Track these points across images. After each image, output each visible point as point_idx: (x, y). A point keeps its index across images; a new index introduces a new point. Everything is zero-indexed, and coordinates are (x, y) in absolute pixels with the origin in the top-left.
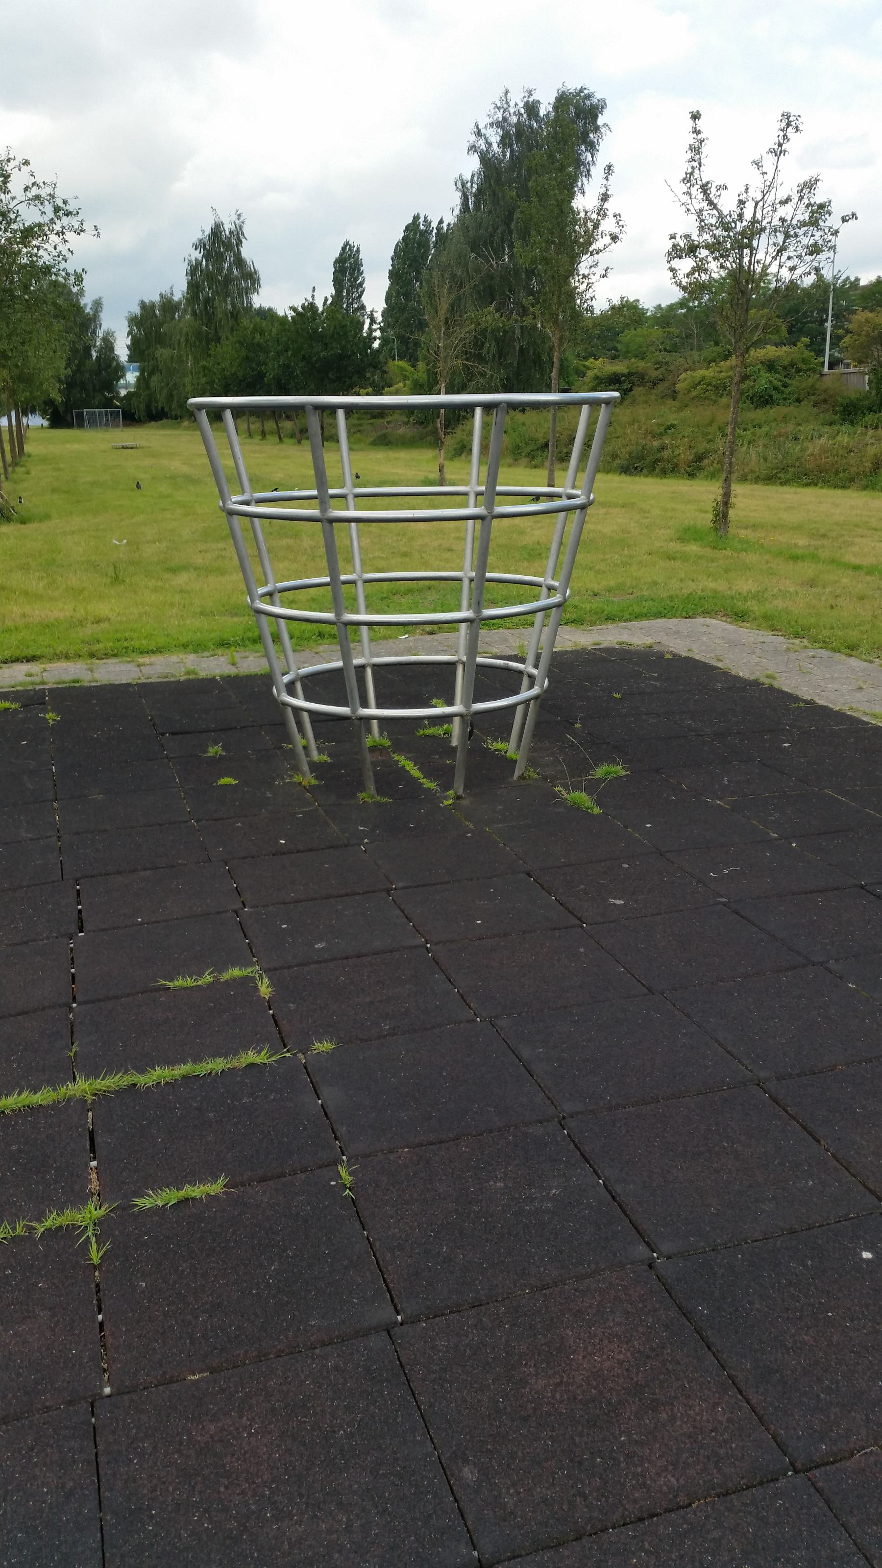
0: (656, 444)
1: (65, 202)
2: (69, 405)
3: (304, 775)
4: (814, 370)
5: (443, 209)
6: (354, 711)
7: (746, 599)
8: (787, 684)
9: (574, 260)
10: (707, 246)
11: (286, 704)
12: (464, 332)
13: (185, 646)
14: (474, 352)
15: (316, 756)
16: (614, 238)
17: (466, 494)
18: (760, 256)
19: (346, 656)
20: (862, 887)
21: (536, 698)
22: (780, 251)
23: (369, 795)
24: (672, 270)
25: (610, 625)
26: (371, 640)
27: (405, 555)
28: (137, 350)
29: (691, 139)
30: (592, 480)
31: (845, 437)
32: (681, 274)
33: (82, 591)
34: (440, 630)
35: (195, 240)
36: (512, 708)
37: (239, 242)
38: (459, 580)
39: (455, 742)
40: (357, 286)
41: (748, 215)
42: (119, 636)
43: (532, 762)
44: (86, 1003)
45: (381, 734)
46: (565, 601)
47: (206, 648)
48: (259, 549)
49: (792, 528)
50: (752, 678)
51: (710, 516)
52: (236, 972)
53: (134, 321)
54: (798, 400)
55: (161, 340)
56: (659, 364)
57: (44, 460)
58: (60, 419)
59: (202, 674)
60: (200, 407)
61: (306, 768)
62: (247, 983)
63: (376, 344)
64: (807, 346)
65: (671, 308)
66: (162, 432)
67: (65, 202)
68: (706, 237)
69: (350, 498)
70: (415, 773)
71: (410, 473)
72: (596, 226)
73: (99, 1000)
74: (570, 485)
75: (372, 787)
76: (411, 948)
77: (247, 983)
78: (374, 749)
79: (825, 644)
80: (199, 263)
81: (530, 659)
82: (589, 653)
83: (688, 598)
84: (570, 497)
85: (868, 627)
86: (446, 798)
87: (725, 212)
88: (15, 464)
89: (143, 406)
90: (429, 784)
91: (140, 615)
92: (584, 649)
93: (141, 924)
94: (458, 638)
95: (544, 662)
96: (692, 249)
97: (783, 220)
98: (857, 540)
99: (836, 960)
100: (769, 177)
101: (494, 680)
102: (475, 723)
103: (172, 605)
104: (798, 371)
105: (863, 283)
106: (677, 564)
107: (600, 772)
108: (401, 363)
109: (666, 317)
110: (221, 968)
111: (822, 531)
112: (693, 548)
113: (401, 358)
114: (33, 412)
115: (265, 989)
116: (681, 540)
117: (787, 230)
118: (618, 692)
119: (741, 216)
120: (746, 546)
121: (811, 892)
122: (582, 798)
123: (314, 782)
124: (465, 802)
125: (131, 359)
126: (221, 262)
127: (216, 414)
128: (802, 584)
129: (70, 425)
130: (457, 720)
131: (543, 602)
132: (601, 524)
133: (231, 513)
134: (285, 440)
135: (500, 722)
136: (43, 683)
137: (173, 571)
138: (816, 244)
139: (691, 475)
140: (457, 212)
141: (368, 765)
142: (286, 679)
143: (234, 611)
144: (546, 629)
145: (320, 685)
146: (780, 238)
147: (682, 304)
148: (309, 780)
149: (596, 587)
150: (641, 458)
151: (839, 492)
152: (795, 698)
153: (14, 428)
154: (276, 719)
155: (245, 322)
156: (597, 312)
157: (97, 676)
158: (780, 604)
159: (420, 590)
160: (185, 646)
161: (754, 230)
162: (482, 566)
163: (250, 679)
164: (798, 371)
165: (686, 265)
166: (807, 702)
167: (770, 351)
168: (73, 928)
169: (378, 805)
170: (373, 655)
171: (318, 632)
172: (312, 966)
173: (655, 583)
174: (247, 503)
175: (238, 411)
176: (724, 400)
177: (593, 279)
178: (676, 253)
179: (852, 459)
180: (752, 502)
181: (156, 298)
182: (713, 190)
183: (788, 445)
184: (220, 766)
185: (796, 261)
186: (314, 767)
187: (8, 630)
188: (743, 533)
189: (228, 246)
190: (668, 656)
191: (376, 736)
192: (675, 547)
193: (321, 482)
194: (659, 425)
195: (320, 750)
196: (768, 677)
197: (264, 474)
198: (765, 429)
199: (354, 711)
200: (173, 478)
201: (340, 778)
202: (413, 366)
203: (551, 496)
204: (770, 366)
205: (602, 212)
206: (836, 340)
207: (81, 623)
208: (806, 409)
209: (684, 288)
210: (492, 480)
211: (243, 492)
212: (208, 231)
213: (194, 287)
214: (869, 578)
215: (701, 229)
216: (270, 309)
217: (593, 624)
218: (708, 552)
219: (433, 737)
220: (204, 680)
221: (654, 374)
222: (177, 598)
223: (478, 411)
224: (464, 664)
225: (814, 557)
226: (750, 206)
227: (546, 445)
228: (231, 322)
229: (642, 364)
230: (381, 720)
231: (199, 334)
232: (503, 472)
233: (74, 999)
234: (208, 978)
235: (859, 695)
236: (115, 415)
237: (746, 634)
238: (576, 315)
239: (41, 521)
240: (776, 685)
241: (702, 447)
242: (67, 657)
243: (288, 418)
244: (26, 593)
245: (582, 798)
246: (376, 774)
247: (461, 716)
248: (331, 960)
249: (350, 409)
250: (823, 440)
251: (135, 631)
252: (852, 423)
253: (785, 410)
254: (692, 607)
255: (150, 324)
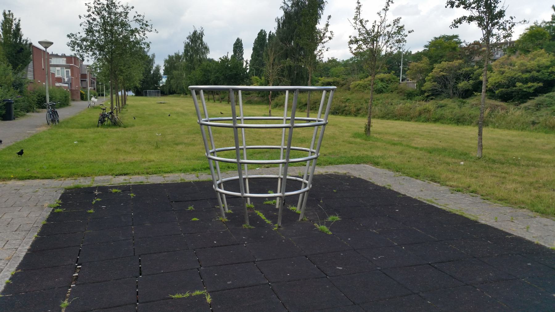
0: (343, 105)
1: (147, 22)
2: (142, 89)
3: (223, 217)
4: (397, 82)
5: (271, 28)
6: (242, 194)
7: (378, 158)
8: (395, 188)
9: (316, 45)
10: (361, 40)
11: (217, 192)
12: (278, 68)
13: (181, 170)
14: (281, 74)
15: (227, 211)
16: (330, 38)
17: (282, 119)
18: (380, 43)
19: (240, 175)
20: (430, 264)
21: (307, 191)
22: (387, 42)
23: (246, 225)
24: (350, 47)
25: (330, 166)
26: (248, 169)
27: (258, 140)
28: (167, 71)
29: (357, 5)
30: (327, 116)
31: (409, 104)
32: (353, 50)
33: (145, 151)
34: (271, 166)
35: (187, 36)
36: (298, 194)
37: (202, 36)
38: (280, 149)
39: (277, 207)
40: (241, 52)
41: (376, 30)
42: (157, 166)
43: (305, 214)
44: (142, 303)
45: (251, 203)
46: (318, 157)
47: (188, 171)
48: (210, 137)
49: (392, 134)
50: (383, 186)
51: (364, 129)
52: (198, 292)
53: (166, 61)
54: (392, 92)
55: (175, 68)
56: (344, 79)
57: (132, 107)
58: (139, 93)
59: (187, 180)
60: (193, 89)
61: (224, 215)
62: (202, 297)
63: (248, 71)
64: (394, 74)
65: (347, 61)
66: (176, 98)
67: (147, 22)
68: (361, 37)
69: (242, 120)
70: (263, 217)
71: (259, 113)
72: (324, 34)
73: (147, 302)
74: (318, 117)
75: (248, 222)
76: (263, 284)
77: (202, 297)
78: (249, 208)
79: (408, 175)
80: (189, 44)
81: (305, 177)
82: (324, 175)
83: (358, 157)
84: (319, 121)
85: (422, 169)
86: (275, 227)
87: (368, 29)
88: (123, 108)
89: (167, 90)
90: (268, 222)
91: (165, 160)
92: (322, 174)
93: (163, 273)
94: (279, 169)
95: (310, 178)
96: (357, 41)
97: (388, 32)
98: (415, 139)
99: (423, 292)
100: (383, 18)
101: (293, 185)
102: (286, 200)
103: (176, 156)
104: (392, 82)
105: (412, 53)
106: (353, 145)
107: (330, 218)
108: (256, 77)
109: (346, 64)
110: (193, 291)
111: (403, 135)
112: (358, 140)
113: (256, 75)
114: (130, 90)
115: (209, 299)
116: (354, 137)
117: (390, 35)
118: (335, 189)
119: (373, 31)
120: (377, 140)
121: (411, 266)
122: (324, 228)
123: (227, 220)
124: (282, 229)
125: (164, 74)
126: (196, 42)
127: (197, 91)
128: (398, 153)
129: (142, 95)
130: (278, 198)
131: (310, 157)
132: (329, 131)
133: (202, 124)
134: (216, 101)
135: (294, 200)
136: (130, 183)
137: (177, 144)
138: (399, 40)
139: (356, 116)
140: (276, 29)
141: (247, 214)
142: (218, 182)
143: (198, 159)
144: (310, 167)
145: (231, 185)
146: (387, 37)
147: (351, 59)
148: (225, 219)
149: (325, 153)
150: (339, 109)
151: (407, 122)
152: (399, 194)
153: (120, 98)
154: (213, 197)
155: (203, 63)
156: (324, 61)
157: (149, 180)
158: (390, 160)
159: (263, 152)
160: (181, 170)
161: (378, 35)
162: (289, 145)
163: (203, 182)
164: (392, 82)
165: (354, 46)
166: (403, 195)
167: (382, 75)
168: (138, 274)
169: (250, 228)
170: (249, 175)
171: (228, 166)
172: (226, 291)
173: (346, 152)
174: (207, 121)
175: (205, 90)
176: (366, 91)
177: (323, 51)
178: (351, 42)
179: (411, 111)
180: (377, 125)
181: (174, 54)
182: (364, 22)
183: (389, 106)
184: (192, 214)
185: (392, 45)
186: (227, 214)
187: (118, 164)
188: (375, 135)
189: (199, 38)
190: (352, 177)
191: (249, 204)
192: (353, 139)
193: (234, 114)
194: (344, 99)
195: (229, 209)
196: (388, 185)
197: (215, 112)
198: (381, 101)
199: (242, 194)
200: (177, 113)
201: (236, 219)
202: (261, 78)
203: (309, 121)
204: (382, 80)
205: (326, 30)
206: (404, 71)
207: (144, 162)
208: (394, 94)
209: (354, 54)
210: (293, 116)
211: (206, 118)
212: (192, 33)
213: (186, 51)
214: (421, 152)
215: (360, 35)
216: (212, 59)
217: (325, 165)
218: (364, 141)
219: (269, 204)
220: (187, 183)
221: (342, 82)
222: (178, 154)
223: (287, 92)
224: (282, 179)
225: (401, 144)
226: (376, 27)
227: (306, 105)
228: (199, 63)
229: (338, 79)
230: (251, 198)
231: (187, 67)
232: (297, 113)
233: (138, 301)
234: (187, 295)
235: (421, 193)
236: (158, 92)
237: (379, 170)
238: (317, 63)
239: (131, 127)
240: (391, 188)
241: (359, 106)
242: (139, 174)
243: (217, 94)
244: (125, 152)
245: (324, 228)
246: (249, 217)
247: (280, 197)
248: (234, 289)
249: (242, 90)
250: (401, 105)
251: (163, 165)
252: (411, 99)
253: (387, 95)
254: (360, 160)
255: (172, 63)
